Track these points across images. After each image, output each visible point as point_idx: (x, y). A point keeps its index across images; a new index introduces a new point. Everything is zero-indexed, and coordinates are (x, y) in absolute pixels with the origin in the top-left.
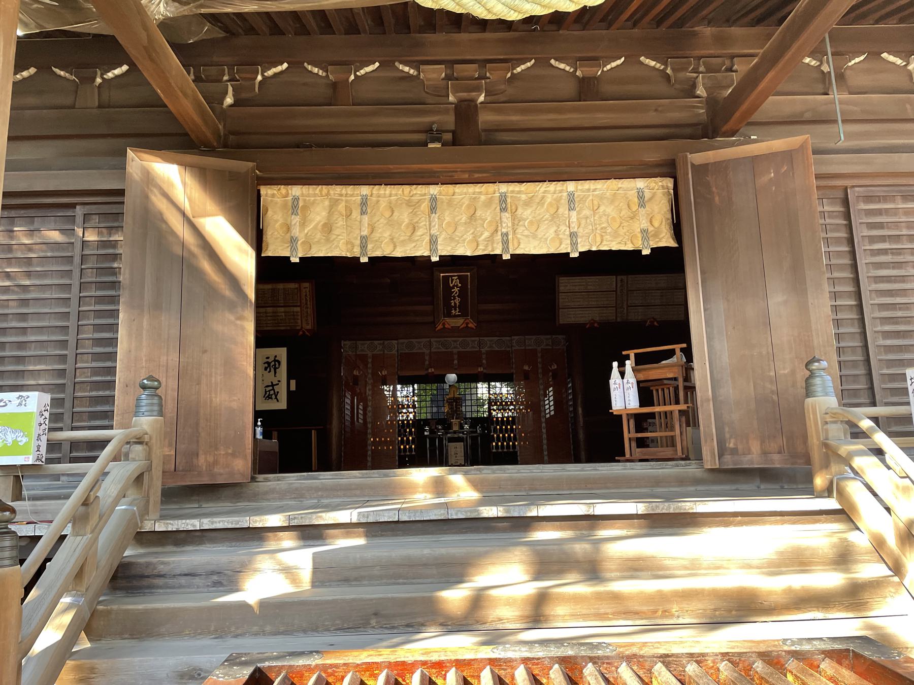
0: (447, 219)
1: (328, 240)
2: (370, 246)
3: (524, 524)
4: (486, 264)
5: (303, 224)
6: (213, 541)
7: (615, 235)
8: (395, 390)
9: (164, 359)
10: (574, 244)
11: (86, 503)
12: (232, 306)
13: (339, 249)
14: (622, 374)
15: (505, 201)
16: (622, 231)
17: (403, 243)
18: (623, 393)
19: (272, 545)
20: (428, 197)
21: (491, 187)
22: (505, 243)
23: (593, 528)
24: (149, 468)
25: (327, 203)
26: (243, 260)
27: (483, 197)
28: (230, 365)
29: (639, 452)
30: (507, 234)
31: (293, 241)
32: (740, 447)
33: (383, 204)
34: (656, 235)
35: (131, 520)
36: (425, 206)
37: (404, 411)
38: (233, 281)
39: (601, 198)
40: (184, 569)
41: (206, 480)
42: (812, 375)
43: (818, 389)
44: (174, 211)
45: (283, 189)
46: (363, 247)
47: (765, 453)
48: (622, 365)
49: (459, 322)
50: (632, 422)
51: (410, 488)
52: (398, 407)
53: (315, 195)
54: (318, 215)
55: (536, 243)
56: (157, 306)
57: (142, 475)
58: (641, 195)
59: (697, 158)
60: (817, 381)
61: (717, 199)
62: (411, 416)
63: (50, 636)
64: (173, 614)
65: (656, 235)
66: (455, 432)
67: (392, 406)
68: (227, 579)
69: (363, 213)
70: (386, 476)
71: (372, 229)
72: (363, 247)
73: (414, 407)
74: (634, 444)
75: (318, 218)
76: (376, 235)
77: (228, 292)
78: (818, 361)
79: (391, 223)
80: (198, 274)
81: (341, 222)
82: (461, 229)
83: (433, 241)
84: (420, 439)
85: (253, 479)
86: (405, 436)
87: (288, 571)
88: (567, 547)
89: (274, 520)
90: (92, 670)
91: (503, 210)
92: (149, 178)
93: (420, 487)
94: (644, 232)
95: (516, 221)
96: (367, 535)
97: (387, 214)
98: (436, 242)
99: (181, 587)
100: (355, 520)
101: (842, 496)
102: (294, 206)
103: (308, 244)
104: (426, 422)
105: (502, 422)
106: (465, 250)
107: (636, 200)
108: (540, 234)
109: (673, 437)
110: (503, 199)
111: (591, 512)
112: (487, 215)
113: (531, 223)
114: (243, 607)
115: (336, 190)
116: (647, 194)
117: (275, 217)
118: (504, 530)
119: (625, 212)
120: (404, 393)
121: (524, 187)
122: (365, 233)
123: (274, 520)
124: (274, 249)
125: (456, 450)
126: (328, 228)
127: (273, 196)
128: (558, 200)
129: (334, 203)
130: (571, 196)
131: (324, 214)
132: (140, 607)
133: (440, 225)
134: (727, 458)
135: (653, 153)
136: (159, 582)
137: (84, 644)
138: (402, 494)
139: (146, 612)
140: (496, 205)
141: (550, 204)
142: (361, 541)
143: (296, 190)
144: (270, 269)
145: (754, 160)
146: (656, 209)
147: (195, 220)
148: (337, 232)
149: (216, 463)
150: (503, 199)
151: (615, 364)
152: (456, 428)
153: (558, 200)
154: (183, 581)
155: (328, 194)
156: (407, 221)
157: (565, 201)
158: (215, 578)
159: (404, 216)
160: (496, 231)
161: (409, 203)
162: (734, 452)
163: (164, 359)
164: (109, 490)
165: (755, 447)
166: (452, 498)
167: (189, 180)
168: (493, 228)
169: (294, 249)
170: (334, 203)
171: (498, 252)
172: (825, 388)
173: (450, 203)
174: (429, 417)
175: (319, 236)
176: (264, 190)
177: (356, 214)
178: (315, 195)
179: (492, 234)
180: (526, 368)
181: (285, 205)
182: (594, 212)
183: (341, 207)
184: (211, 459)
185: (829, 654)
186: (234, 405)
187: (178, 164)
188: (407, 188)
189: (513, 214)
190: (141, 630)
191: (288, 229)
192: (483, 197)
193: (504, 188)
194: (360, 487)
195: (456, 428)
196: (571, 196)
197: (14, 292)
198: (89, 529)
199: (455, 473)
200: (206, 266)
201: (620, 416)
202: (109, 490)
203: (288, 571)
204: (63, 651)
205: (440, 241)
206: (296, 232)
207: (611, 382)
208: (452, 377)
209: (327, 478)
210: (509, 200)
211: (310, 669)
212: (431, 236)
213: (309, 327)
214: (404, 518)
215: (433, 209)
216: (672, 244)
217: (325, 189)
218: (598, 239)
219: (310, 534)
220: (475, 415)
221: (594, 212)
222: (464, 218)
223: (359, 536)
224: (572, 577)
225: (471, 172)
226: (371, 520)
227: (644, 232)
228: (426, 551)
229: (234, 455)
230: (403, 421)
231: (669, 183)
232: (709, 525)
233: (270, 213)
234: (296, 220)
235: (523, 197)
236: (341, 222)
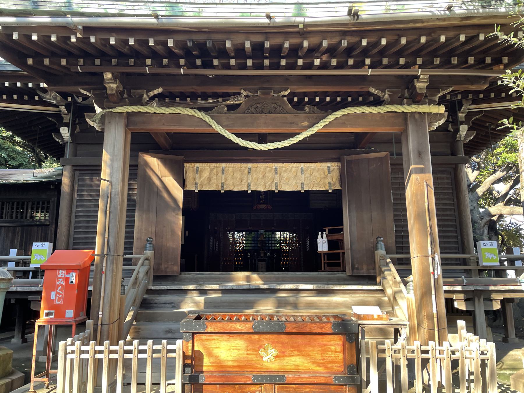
0: (255, 176)
1: (209, 184)
2: (225, 187)
3: (274, 291)
4: (269, 194)
5: (200, 178)
6: (171, 294)
7: (319, 184)
8: (233, 235)
9: (150, 229)
10: (303, 187)
11: (136, 279)
12: (174, 210)
13: (213, 187)
14: (322, 237)
15: (277, 170)
16: (321, 183)
17: (238, 185)
18: (323, 245)
19: (190, 295)
20: (247, 168)
21: (271, 165)
22: (276, 186)
23: (298, 293)
24: (150, 269)
25: (209, 169)
26: (178, 193)
27: (268, 169)
28: (173, 232)
29: (327, 268)
30: (277, 183)
31: (196, 184)
32: (359, 267)
33: (231, 170)
34: (334, 185)
35: (146, 285)
36: (246, 171)
37: (238, 245)
38: (175, 200)
39: (314, 170)
40: (163, 302)
41: (164, 274)
42: (378, 243)
43: (379, 248)
44: (155, 175)
45: (193, 164)
46: (222, 187)
47: (368, 270)
48: (322, 234)
49: (264, 206)
50: (326, 256)
51: (238, 279)
52: (235, 242)
53: (205, 167)
54: (206, 174)
55: (288, 187)
56: (148, 210)
57: (148, 271)
58: (329, 169)
59: (349, 158)
60: (379, 245)
61: (355, 173)
62: (242, 248)
63: (128, 319)
64: (162, 314)
65: (334, 185)
66: (262, 257)
67: (232, 242)
68: (177, 305)
69: (223, 174)
70: (229, 274)
71: (226, 180)
72: (222, 187)
73: (243, 243)
74: (326, 265)
75: (206, 175)
76: (227, 182)
77: (172, 204)
78: (380, 238)
79: (233, 177)
80: (162, 197)
81: (214, 177)
82: (260, 180)
83: (249, 185)
84: (245, 259)
85: (180, 274)
86: (238, 257)
87: (196, 303)
88: (287, 298)
89: (191, 287)
90: (139, 329)
91: (276, 173)
92: (147, 164)
93: (240, 278)
94: (329, 183)
95: (281, 178)
96: (222, 293)
97: (232, 174)
98: (250, 185)
99: (162, 307)
100: (218, 288)
101: (383, 286)
102: (197, 171)
103: (202, 185)
104: (249, 251)
105: (286, 252)
106: (261, 189)
107: (327, 171)
108: (290, 183)
109: (340, 263)
110: (276, 169)
111: (298, 288)
112: (270, 175)
113: (287, 179)
114: (183, 312)
115: (213, 165)
116: (331, 169)
117: (190, 175)
118: (268, 293)
119: (322, 176)
120: (238, 236)
121: (284, 165)
122: (223, 181)
123: (191, 287)
124: (190, 187)
125: (262, 264)
126: (209, 179)
127: (189, 167)
128: (297, 170)
129: (212, 170)
130: (302, 168)
131: (208, 174)
132: (152, 312)
133: (252, 179)
134: (355, 271)
135: (333, 154)
136: (155, 305)
137: (135, 323)
138: (234, 281)
139: (153, 313)
140: (273, 172)
141: (294, 172)
142: (220, 295)
143: (198, 165)
144: (187, 194)
145: (369, 160)
146: (335, 174)
147: (163, 179)
148: (213, 181)
149: (167, 267)
150: (276, 169)
151: (320, 233)
152: (262, 255)
153: (297, 170)
154: (163, 305)
155: (210, 166)
156: (239, 177)
157: (299, 171)
158: (173, 305)
159: (238, 175)
160: (273, 181)
161: (240, 170)
162: (357, 269)
163: (150, 229)
164: (141, 275)
165: (365, 267)
166: (253, 283)
167: (160, 163)
168: (272, 180)
169: (196, 187)
170: (212, 170)
171: (273, 190)
172: (381, 247)
173: (256, 170)
174: (251, 248)
175: (206, 182)
176: (185, 165)
177: (220, 174)
178: (205, 167)
179: (271, 183)
180: (294, 228)
181: (193, 170)
182: (311, 175)
183: (215, 171)
184: (166, 266)
185: (333, 316)
186: (174, 246)
187: (156, 158)
188: (239, 165)
189: (280, 175)
190: (152, 319)
191: (195, 179)
192: (268, 169)
193: (276, 165)
194: (219, 278)
195: (262, 255)
196: (302, 168)
197: (93, 202)
198: (137, 286)
199: (254, 274)
200: (165, 195)
201: (321, 254)
202: (141, 275)
203: (196, 303)
204: (131, 321)
205: (251, 185)
206: (197, 180)
207: (318, 240)
208: (262, 231)
209: (207, 274)
210: (278, 170)
211: (210, 315)
212: (248, 183)
213: (195, 207)
214: (235, 288)
215: (249, 173)
216: (340, 188)
217: (208, 164)
218: (312, 186)
219: (203, 292)
220: (273, 248)
221: (311, 175)
222: (261, 176)
223: (219, 293)
224: (289, 308)
225: (264, 159)
226: (224, 288)
227: (329, 183)
228: (241, 298)
229: (174, 265)
230: (237, 250)
231: (339, 164)
232: (339, 293)
233: (188, 173)
234: (197, 176)
235: (284, 168)
236: (214, 177)
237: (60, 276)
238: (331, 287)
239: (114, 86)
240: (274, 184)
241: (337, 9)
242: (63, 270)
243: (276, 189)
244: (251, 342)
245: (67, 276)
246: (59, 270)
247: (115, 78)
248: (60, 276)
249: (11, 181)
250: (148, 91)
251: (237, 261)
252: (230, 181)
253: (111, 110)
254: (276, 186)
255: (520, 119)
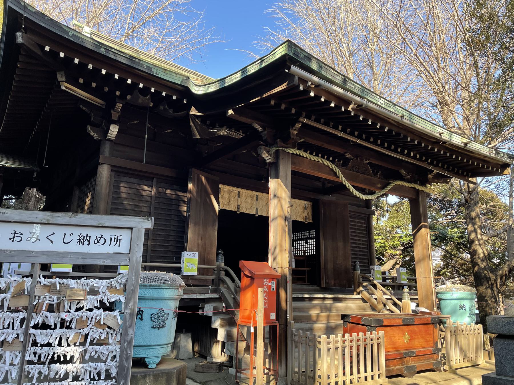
83: (257, 210)
159: (249, 200)
177: (237, 197)
215: (257, 200)
232: (345, 301)
237: (265, 284)
238: (340, 296)
241: (427, 124)
242: (266, 278)
245: (270, 284)
246: (264, 278)
248: (265, 284)
252: (243, 205)
253: (284, 149)
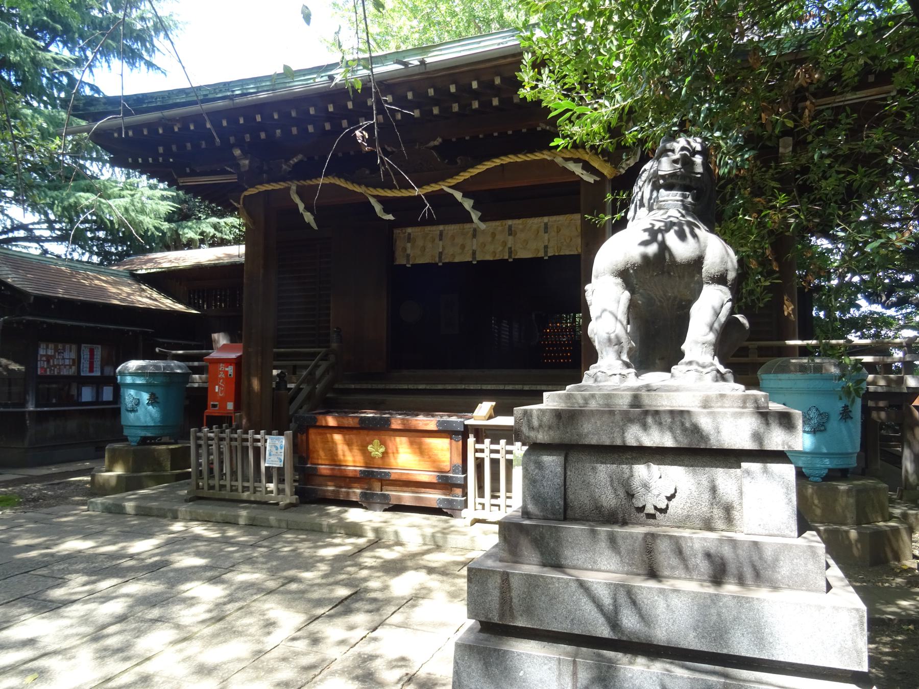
10: (546, 252)
71: (443, 248)
72: (440, 257)
83: (474, 253)
102: (409, 239)
103: (453, 255)
130: (546, 225)
150: (510, 227)
169: (408, 260)
171: (506, 257)
196: (546, 225)
234: (409, 245)
239: (247, 162)
240: (507, 250)
243: (510, 257)
244: (720, 631)
247: (245, 154)
249: (524, 254)
250: (287, 160)
251: (568, 358)
254: (510, 252)
255: (543, 388)
